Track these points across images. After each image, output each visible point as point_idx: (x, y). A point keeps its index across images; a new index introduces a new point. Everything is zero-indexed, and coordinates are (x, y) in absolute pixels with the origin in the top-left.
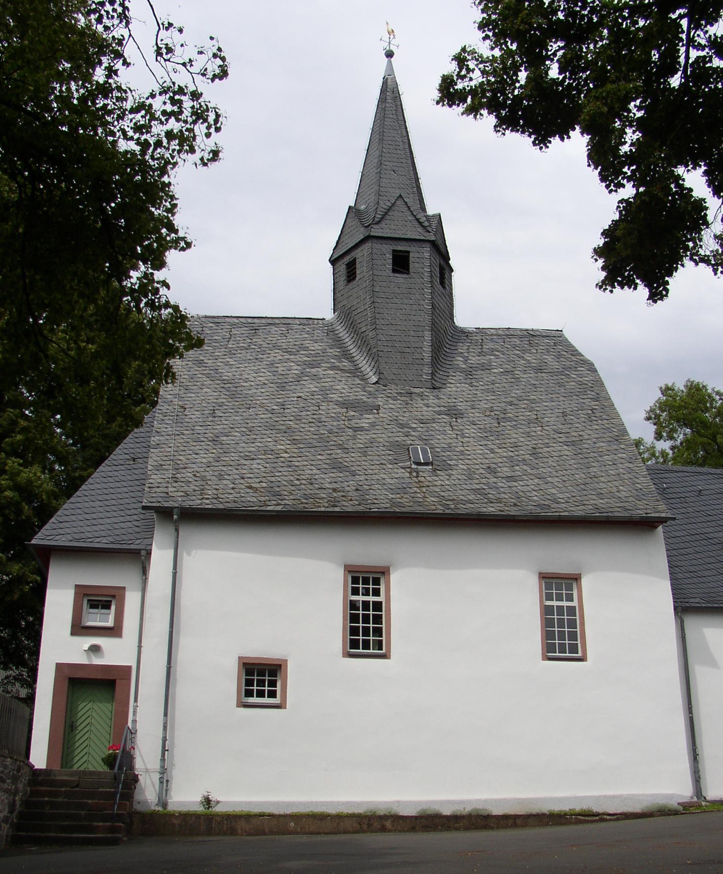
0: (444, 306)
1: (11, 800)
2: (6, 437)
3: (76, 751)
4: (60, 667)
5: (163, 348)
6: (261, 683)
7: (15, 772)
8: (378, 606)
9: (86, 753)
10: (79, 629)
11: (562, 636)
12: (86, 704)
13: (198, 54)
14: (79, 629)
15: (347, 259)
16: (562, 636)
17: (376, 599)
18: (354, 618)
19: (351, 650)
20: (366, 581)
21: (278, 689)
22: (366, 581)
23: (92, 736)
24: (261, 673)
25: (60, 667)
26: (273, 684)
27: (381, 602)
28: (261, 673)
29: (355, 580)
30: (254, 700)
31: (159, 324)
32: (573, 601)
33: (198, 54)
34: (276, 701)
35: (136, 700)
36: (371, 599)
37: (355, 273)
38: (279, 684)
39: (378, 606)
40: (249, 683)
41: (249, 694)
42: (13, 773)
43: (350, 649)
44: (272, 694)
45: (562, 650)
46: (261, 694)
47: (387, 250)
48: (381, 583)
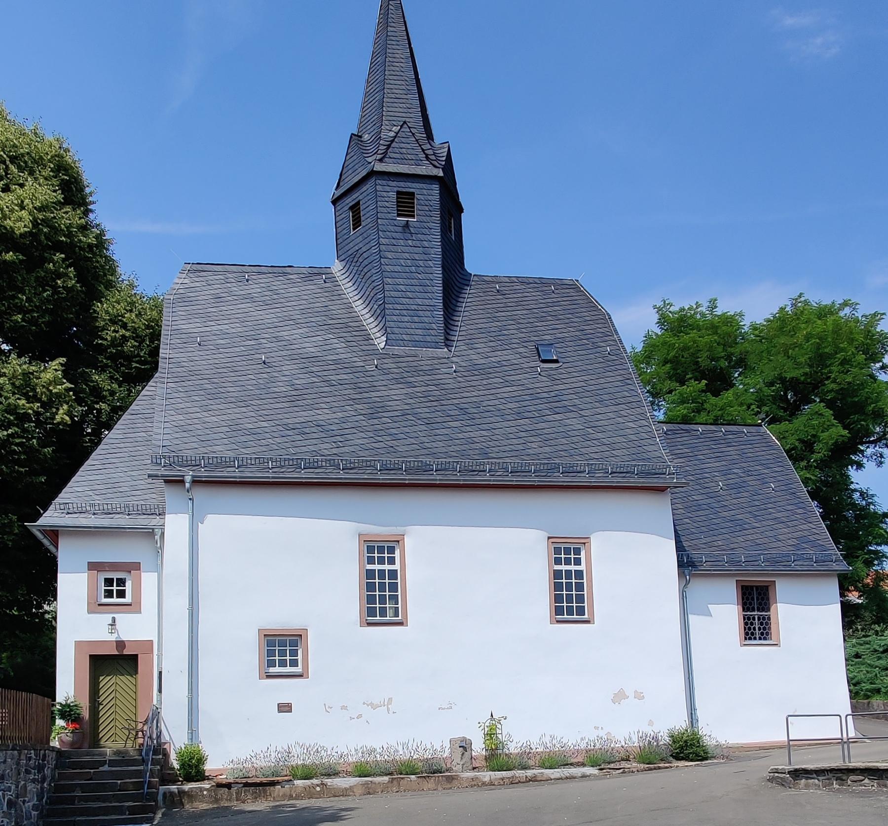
0: (455, 255)
1: (39, 789)
2: (100, 303)
3: (100, 727)
4: (78, 644)
5: (147, 331)
6: (282, 653)
7: (41, 761)
8: (393, 574)
9: (113, 719)
10: (96, 607)
11: (569, 599)
12: (110, 677)
13: (280, 711)
14: (96, 607)
15: (350, 201)
16: (569, 599)
17: (392, 567)
18: (370, 587)
19: (369, 618)
20: (381, 550)
21: (300, 657)
22: (381, 550)
23: (118, 702)
24: (282, 644)
25: (78, 644)
26: (294, 653)
27: (397, 570)
28: (282, 644)
29: (370, 549)
30: (277, 670)
31: (125, 320)
32: (580, 565)
33: (280, 711)
34: (298, 670)
35: (160, 691)
36: (386, 567)
37: (360, 221)
38: (300, 652)
39: (393, 574)
40: (271, 653)
41: (271, 664)
42: (38, 763)
43: (368, 616)
44: (294, 663)
45: (570, 612)
46: (283, 664)
47: (389, 192)
48: (396, 552)
